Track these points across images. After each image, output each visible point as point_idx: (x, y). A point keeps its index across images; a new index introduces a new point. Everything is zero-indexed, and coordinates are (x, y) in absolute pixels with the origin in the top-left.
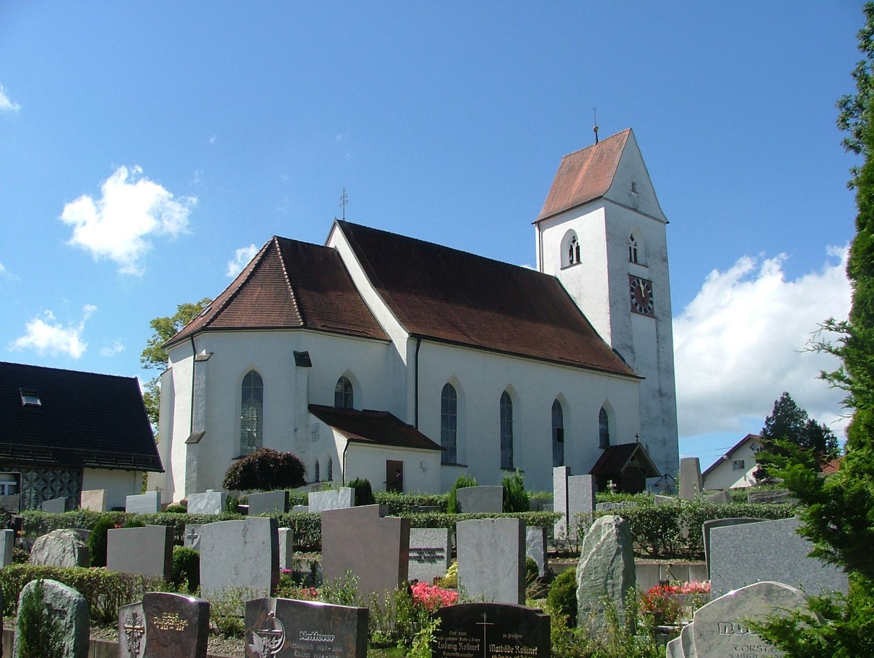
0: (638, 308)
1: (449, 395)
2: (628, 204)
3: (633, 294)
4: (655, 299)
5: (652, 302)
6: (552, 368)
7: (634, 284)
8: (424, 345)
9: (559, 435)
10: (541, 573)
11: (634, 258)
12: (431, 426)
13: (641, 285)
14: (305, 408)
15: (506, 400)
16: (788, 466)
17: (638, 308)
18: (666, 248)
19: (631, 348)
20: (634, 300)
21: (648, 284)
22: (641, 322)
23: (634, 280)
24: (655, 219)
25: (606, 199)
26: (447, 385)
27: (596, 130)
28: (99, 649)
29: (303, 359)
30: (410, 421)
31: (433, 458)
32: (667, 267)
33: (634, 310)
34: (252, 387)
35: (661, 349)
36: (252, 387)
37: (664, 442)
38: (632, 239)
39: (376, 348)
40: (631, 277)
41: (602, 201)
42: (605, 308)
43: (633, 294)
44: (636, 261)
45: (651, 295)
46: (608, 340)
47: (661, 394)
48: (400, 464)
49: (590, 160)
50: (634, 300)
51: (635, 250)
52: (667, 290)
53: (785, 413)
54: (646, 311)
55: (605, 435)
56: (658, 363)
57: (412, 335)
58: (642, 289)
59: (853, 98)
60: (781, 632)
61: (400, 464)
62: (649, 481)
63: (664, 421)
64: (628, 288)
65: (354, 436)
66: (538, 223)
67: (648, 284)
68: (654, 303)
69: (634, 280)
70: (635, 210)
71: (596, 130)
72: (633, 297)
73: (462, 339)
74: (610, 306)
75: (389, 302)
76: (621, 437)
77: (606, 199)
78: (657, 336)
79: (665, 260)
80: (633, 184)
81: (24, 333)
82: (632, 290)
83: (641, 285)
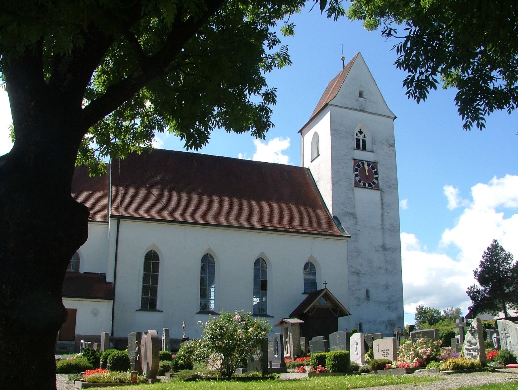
1: (152, 261)
2: (355, 107)
3: (357, 173)
4: (380, 175)
5: (377, 179)
6: (278, 236)
7: (359, 166)
8: (124, 223)
11: (361, 145)
13: (366, 166)
16: (367, 18)
18: (393, 137)
19: (354, 215)
20: (358, 178)
21: (374, 166)
22: (366, 196)
23: (358, 164)
24: (382, 115)
25: (333, 105)
27: (343, 59)
28: (105, 362)
32: (394, 151)
33: (357, 185)
35: (385, 214)
37: (387, 287)
38: (361, 132)
40: (356, 161)
41: (329, 107)
42: (329, 186)
43: (357, 173)
44: (364, 148)
45: (376, 173)
47: (384, 248)
50: (358, 178)
51: (364, 141)
52: (394, 168)
53: (274, 101)
54: (370, 185)
56: (382, 224)
58: (367, 169)
60: (474, 102)
62: (341, 321)
63: (386, 270)
64: (352, 170)
66: (301, 131)
67: (374, 166)
68: (380, 179)
69: (358, 164)
71: (343, 59)
72: (356, 176)
73: (189, 219)
74: (333, 184)
77: (333, 105)
78: (382, 204)
79: (393, 145)
82: (356, 170)
83: (366, 166)
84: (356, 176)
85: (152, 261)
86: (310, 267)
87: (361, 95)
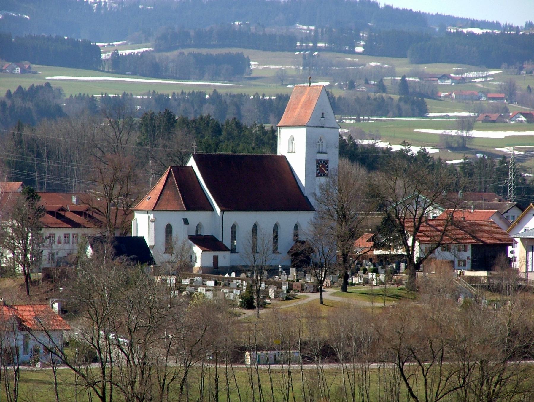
0: (320, 174)
1: (234, 229)
9: (276, 237)
10: (506, 197)
12: (227, 242)
14: (187, 237)
15: (276, 227)
17: (320, 174)
20: (318, 171)
26: (233, 224)
29: (186, 221)
30: (220, 240)
31: (227, 254)
34: (169, 229)
36: (169, 229)
39: (207, 213)
46: (304, 185)
48: (217, 257)
49: (305, 96)
50: (318, 171)
55: (296, 235)
57: (222, 211)
59: (313, 218)
61: (217, 257)
64: (315, 166)
65: (206, 249)
69: (318, 162)
70: (323, 127)
72: (317, 170)
75: (192, 84)
76: (302, 238)
80: (323, 114)
81: (141, 240)
82: (317, 166)
84: (317, 170)
85: (234, 229)
86: (296, 227)
87: (322, 117)
